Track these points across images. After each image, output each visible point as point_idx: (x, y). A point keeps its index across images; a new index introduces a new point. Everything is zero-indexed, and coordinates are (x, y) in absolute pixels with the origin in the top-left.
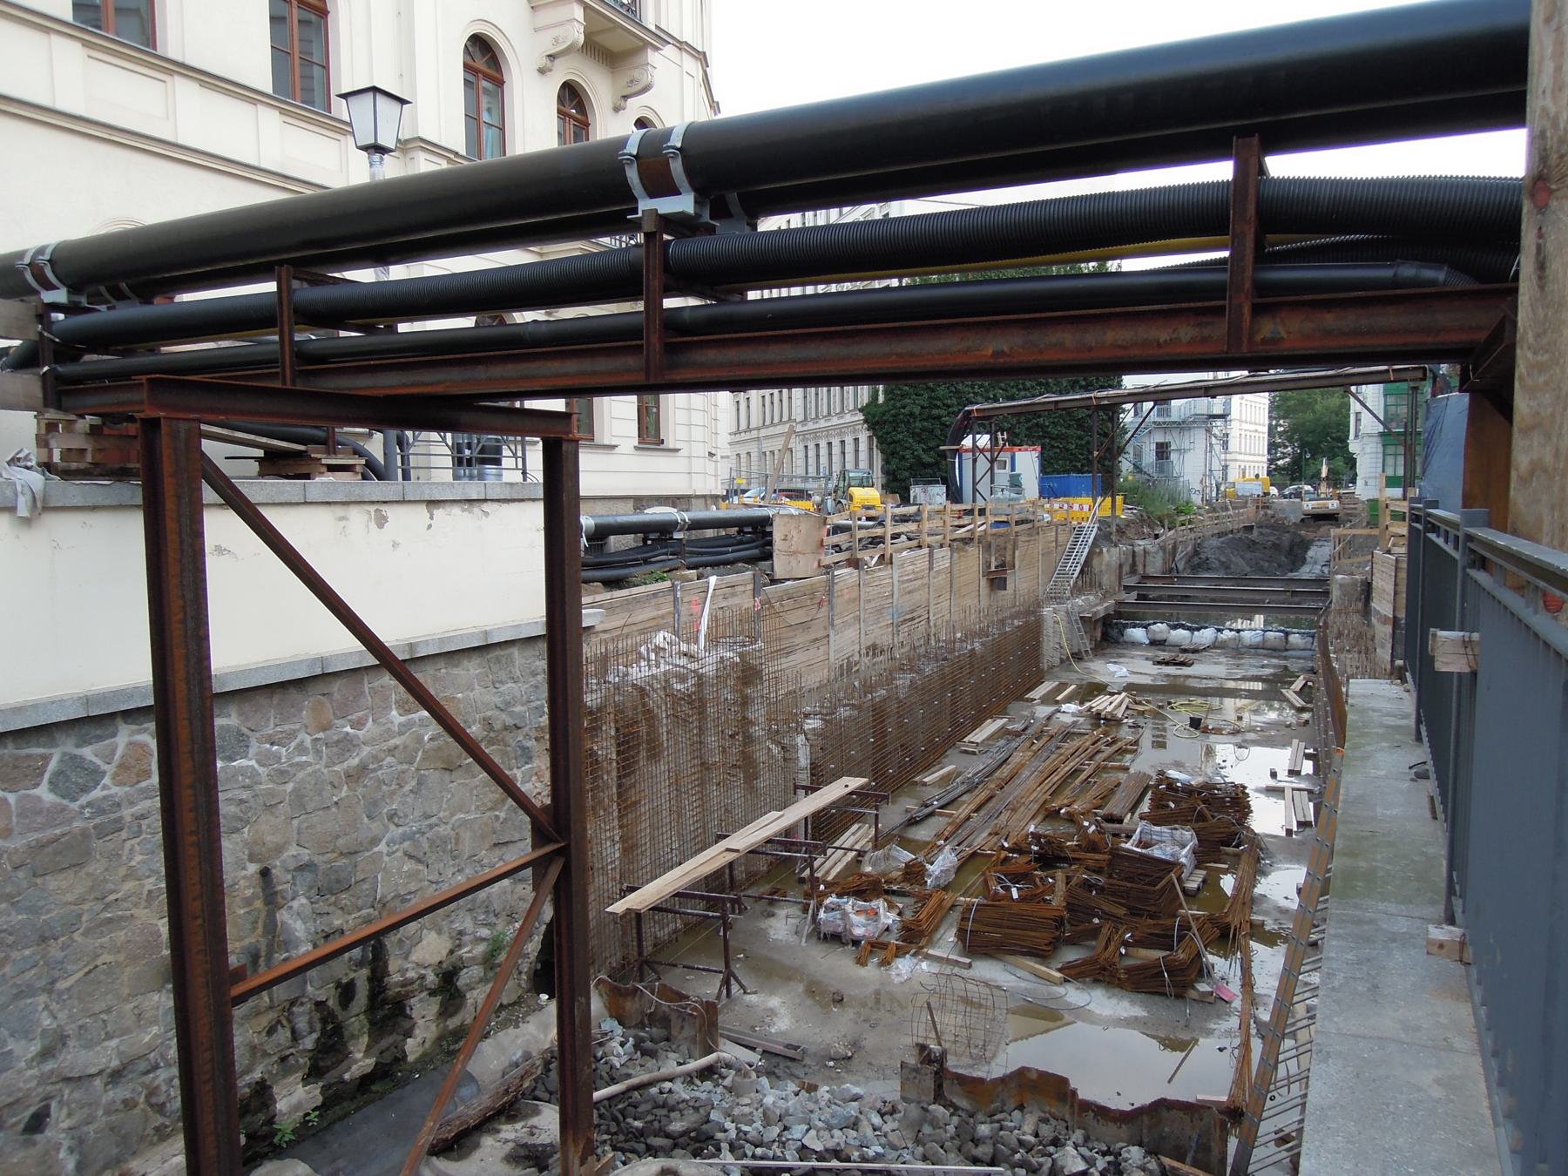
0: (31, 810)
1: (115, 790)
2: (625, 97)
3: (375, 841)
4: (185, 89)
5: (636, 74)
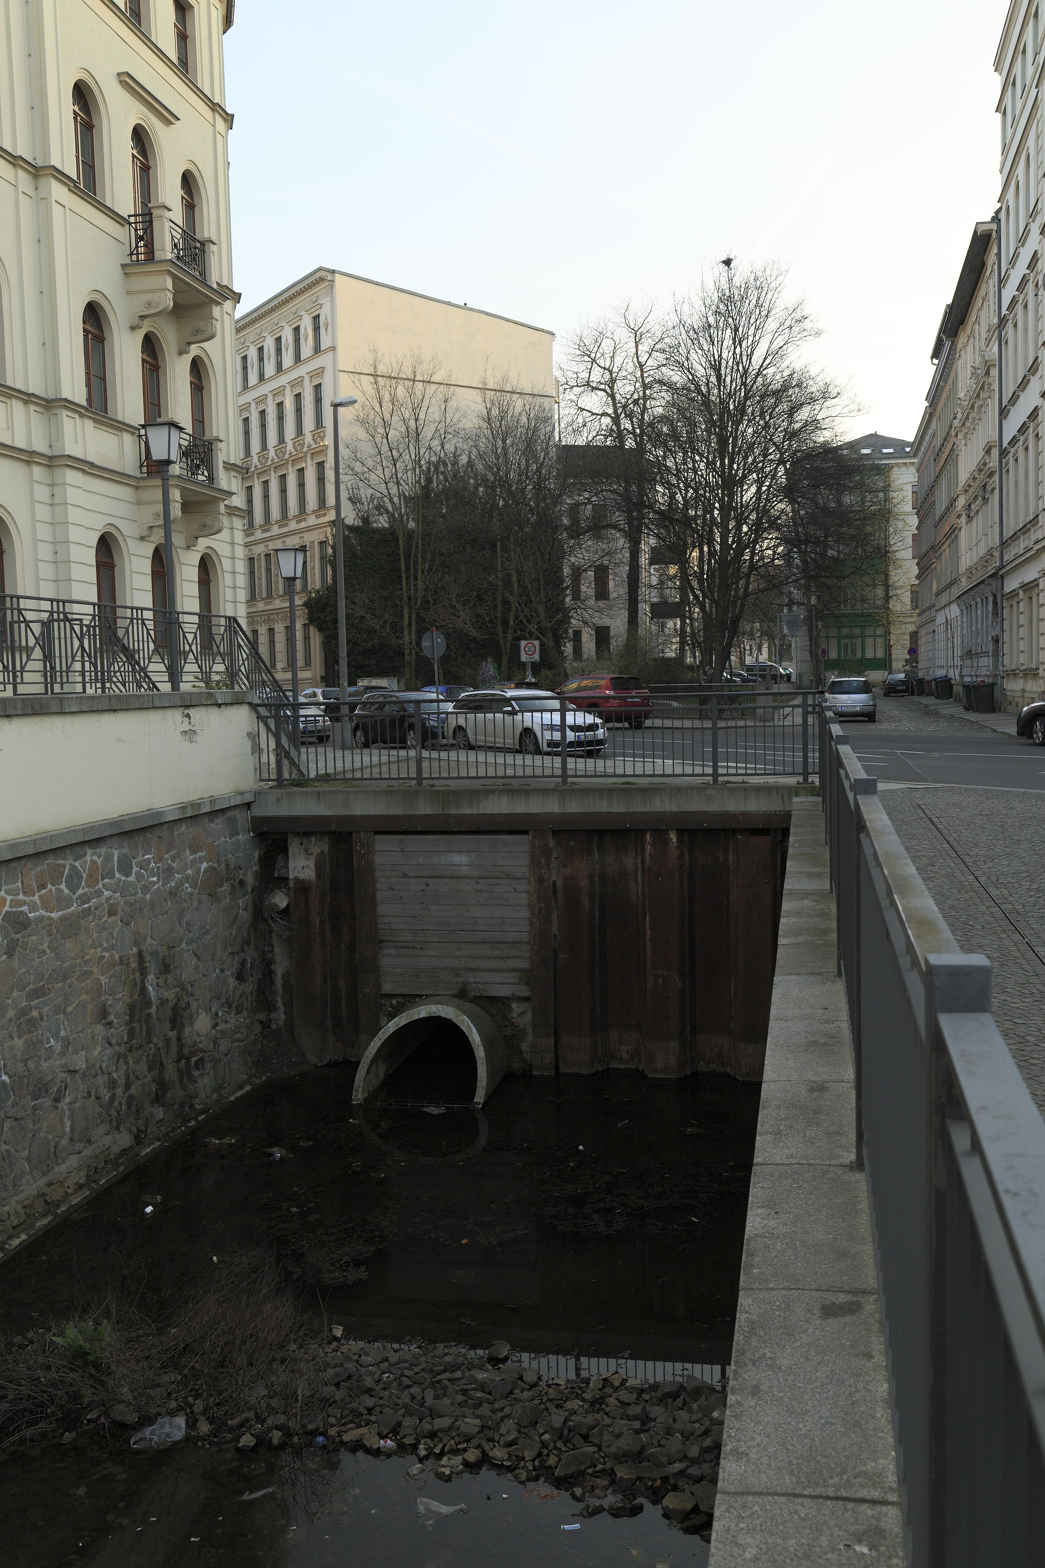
1: (86, 890)
2: (189, 344)
3: (181, 940)
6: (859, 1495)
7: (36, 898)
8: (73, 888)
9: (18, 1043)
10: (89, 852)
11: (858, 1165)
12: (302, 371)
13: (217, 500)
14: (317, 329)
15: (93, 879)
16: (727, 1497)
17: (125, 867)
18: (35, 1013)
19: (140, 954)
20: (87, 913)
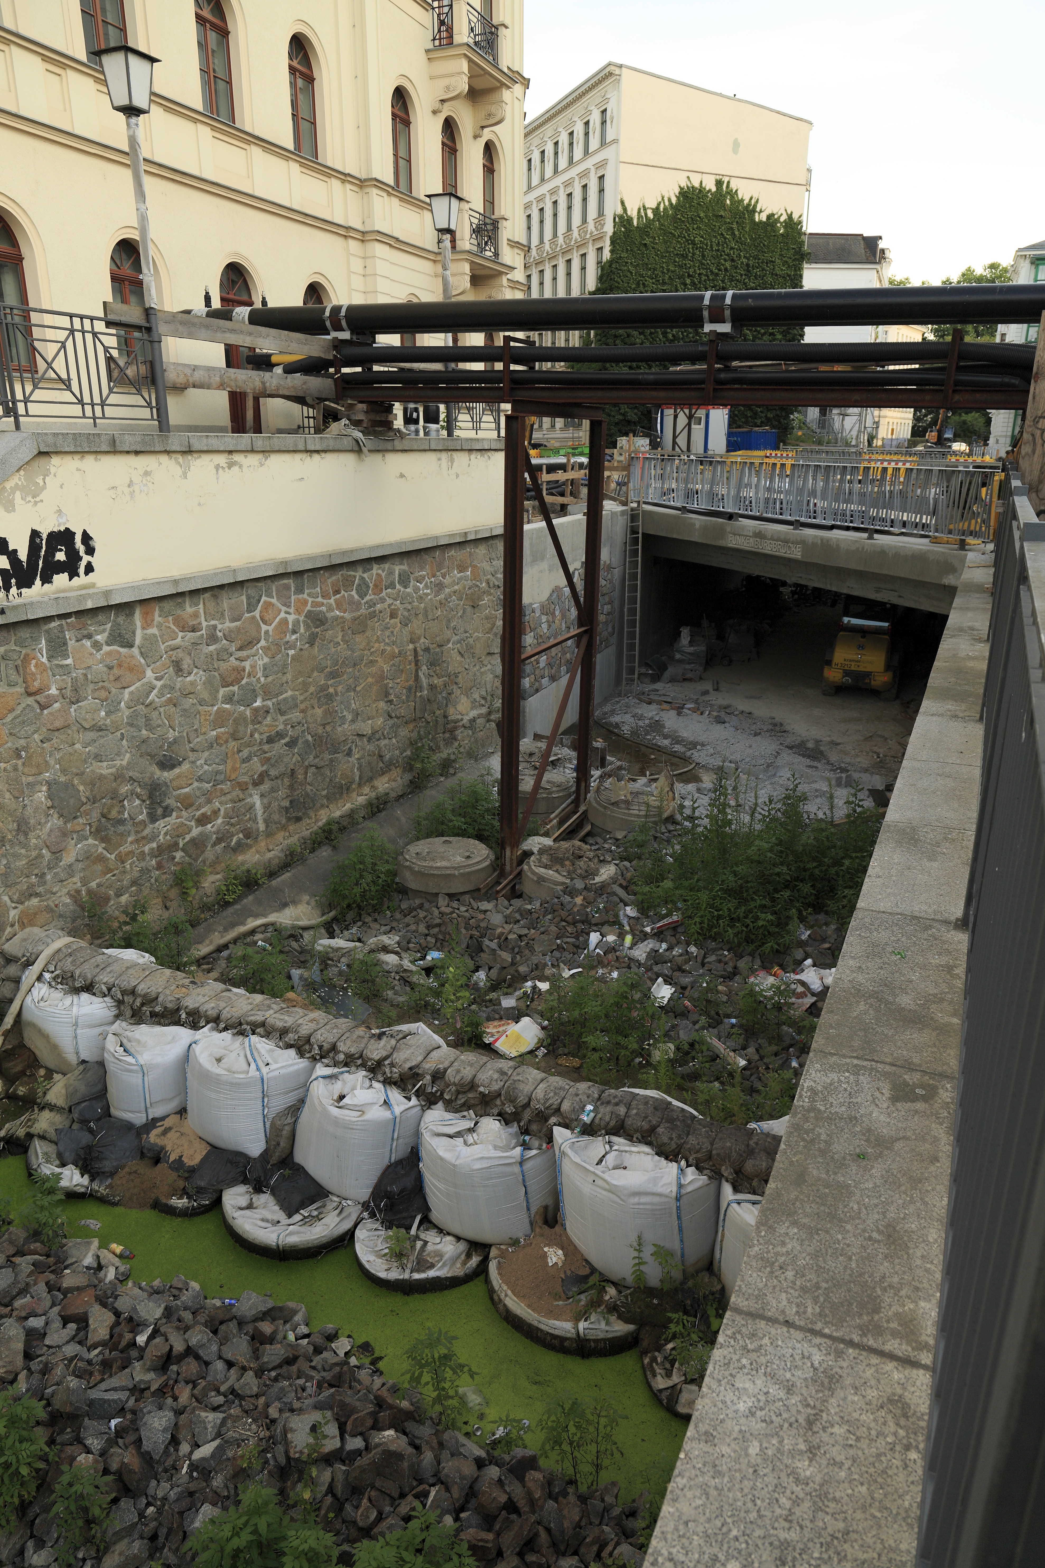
0: (351, 602)
2: (483, 127)
3: (448, 641)
4: (256, 151)
5: (493, 108)
6: (887, 1348)
7: (332, 601)
8: (362, 595)
9: (319, 712)
10: (375, 567)
11: (962, 924)
12: (590, 163)
13: (501, 273)
14: (604, 123)
15: (378, 589)
16: (738, 1318)
17: (404, 580)
18: (331, 690)
19: (415, 650)
20: (372, 615)
